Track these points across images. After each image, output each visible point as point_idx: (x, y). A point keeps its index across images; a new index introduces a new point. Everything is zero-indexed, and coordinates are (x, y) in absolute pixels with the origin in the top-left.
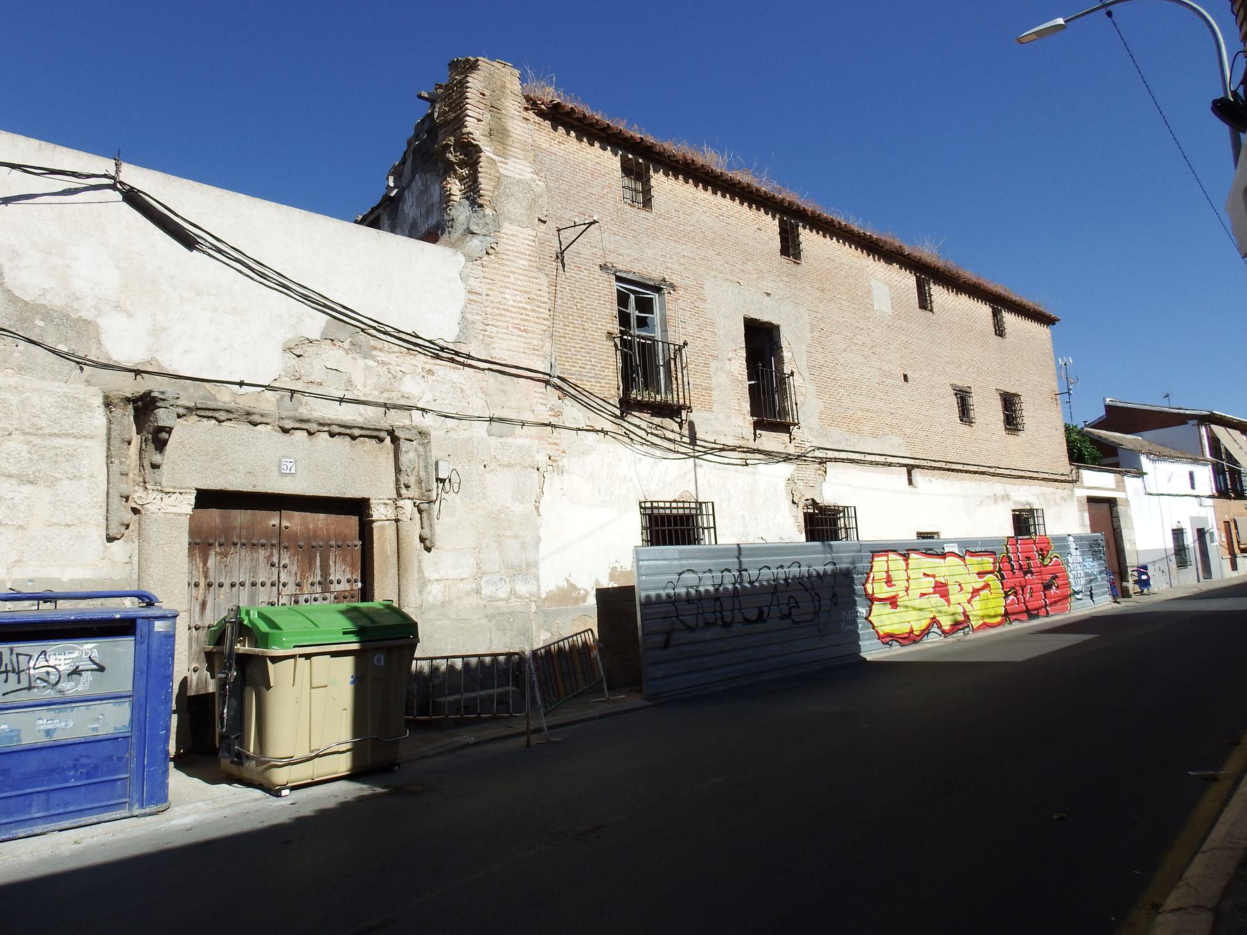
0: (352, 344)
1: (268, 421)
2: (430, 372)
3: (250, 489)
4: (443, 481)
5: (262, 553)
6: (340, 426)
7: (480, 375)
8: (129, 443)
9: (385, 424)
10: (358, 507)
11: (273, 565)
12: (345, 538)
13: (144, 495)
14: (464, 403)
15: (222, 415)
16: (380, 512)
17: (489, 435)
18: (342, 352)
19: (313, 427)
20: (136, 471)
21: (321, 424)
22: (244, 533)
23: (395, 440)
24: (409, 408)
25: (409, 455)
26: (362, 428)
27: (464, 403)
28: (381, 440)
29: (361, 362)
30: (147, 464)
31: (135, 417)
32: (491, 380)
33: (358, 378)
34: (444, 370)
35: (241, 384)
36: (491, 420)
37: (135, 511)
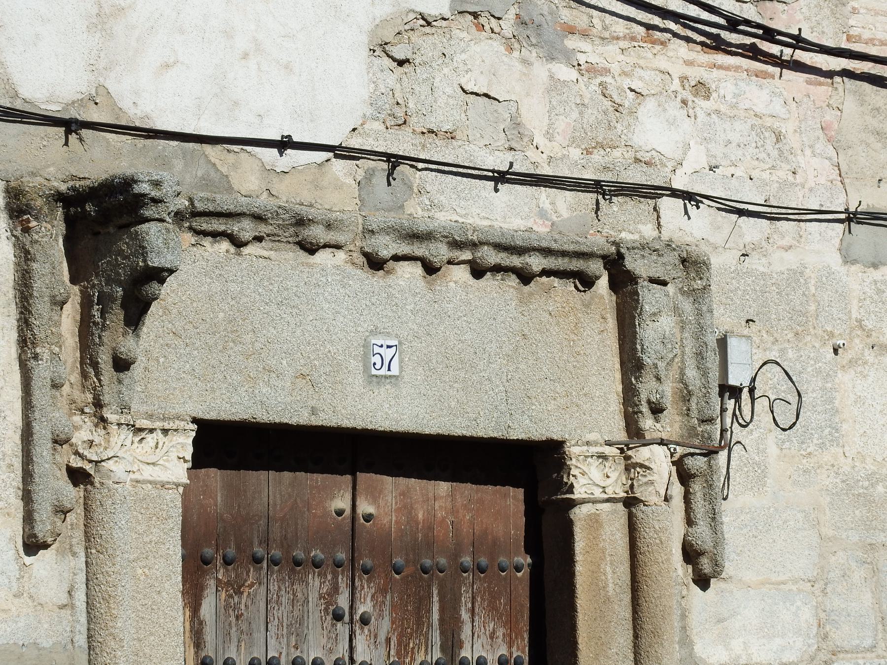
0: (521, 22)
1: (341, 238)
2: (701, 89)
3: (301, 417)
4: (735, 392)
5: (315, 585)
6: (499, 247)
7: (822, 90)
8: (62, 304)
9: (597, 242)
10: (532, 468)
11: (338, 617)
12: (494, 548)
13: (98, 436)
14: (783, 173)
15: (245, 229)
16: (592, 479)
17: (848, 260)
18: (497, 46)
19: (439, 252)
20: (75, 377)
21: (456, 245)
22: (276, 531)
23: (622, 280)
24: (650, 192)
25: (661, 323)
26: (547, 252)
27: (783, 173)
28: (586, 281)
29: (541, 70)
30: (105, 359)
31: (67, 240)
32: (850, 105)
33: (535, 117)
34: (736, 81)
35: (284, 144)
36: (852, 218)
37: (78, 476)
